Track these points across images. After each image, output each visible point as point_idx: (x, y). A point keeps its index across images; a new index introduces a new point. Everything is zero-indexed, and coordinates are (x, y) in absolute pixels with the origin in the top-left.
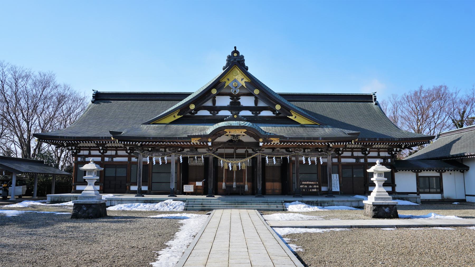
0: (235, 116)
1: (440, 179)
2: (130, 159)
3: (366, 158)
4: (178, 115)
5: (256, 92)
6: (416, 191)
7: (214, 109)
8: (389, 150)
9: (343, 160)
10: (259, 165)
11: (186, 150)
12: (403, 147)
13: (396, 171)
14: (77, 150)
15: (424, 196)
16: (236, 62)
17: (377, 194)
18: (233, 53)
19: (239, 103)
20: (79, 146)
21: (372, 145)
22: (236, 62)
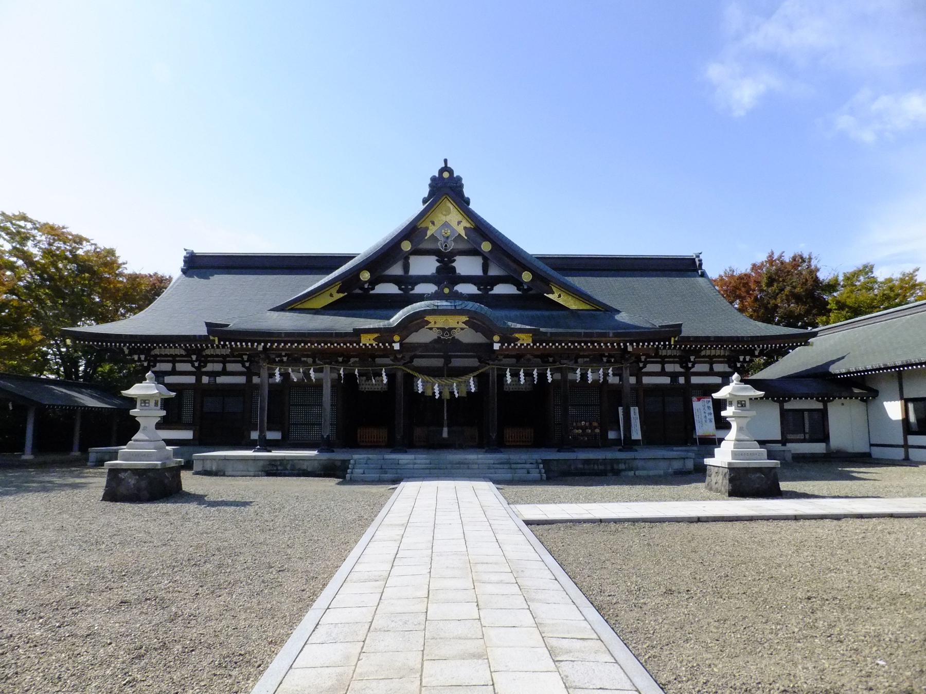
0: (446, 291)
1: (824, 413)
3: (688, 374)
4: (338, 292)
5: (486, 247)
6: (779, 438)
7: (407, 282)
9: (646, 380)
12: (757, 353)
16: (446, 188)
18: (442, 171)
19: (454, 268)
21: (700, 350)
22: (446, 188)
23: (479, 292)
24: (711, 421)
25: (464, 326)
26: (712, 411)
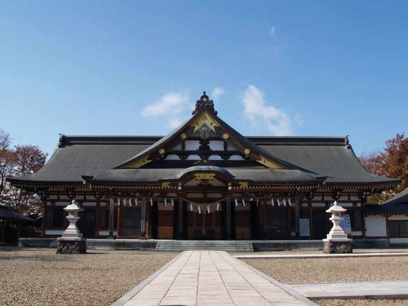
2: (98, 204)
4: (148, 160)
6: (386, 235)
7: (184, 154)
8: (360, 194)
9: (314, 205)
10: (228, 209)
11: (155, 195)
12: (372, 191)
13: (366, 216)
14: (73, 195)
15: (393, 240)
16: (205, 107)
17: (336, 232)
18: (202, 98)
19: (209, 147)
20: (48, 190)
22: (205, 107)
23: (223, 160)
24: (349, 227)
25: (214, 178)
26: (349, 221)
